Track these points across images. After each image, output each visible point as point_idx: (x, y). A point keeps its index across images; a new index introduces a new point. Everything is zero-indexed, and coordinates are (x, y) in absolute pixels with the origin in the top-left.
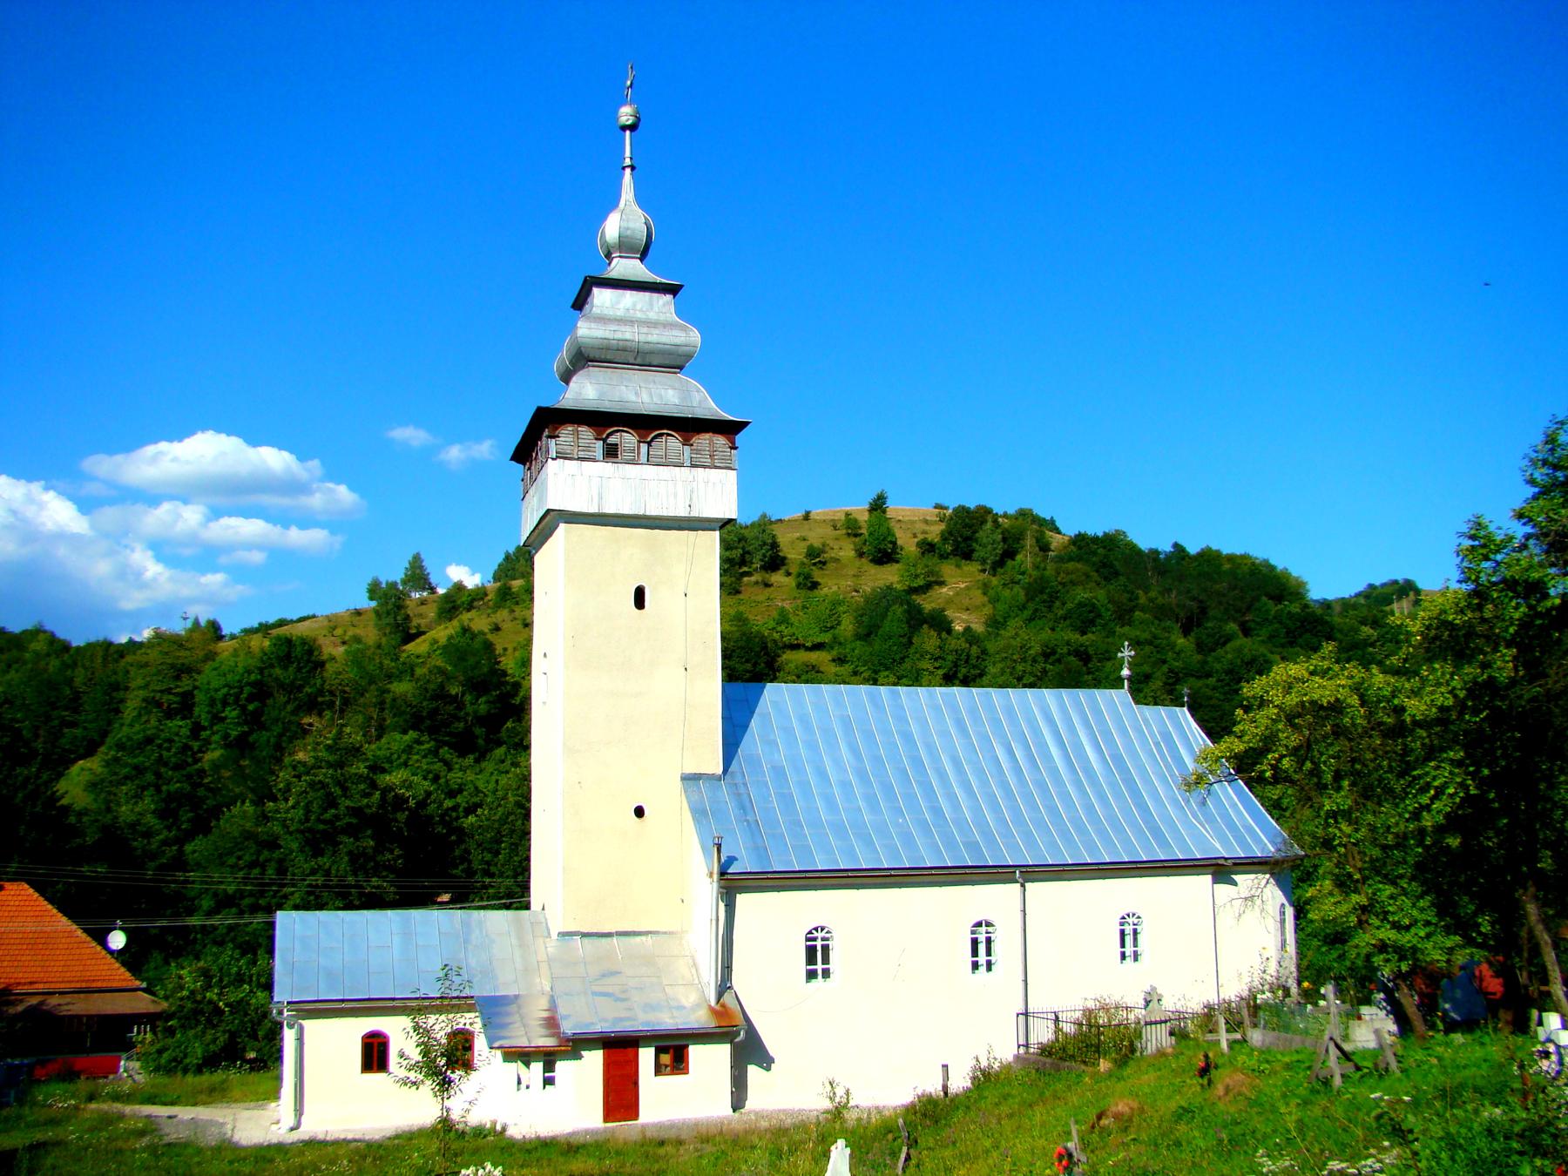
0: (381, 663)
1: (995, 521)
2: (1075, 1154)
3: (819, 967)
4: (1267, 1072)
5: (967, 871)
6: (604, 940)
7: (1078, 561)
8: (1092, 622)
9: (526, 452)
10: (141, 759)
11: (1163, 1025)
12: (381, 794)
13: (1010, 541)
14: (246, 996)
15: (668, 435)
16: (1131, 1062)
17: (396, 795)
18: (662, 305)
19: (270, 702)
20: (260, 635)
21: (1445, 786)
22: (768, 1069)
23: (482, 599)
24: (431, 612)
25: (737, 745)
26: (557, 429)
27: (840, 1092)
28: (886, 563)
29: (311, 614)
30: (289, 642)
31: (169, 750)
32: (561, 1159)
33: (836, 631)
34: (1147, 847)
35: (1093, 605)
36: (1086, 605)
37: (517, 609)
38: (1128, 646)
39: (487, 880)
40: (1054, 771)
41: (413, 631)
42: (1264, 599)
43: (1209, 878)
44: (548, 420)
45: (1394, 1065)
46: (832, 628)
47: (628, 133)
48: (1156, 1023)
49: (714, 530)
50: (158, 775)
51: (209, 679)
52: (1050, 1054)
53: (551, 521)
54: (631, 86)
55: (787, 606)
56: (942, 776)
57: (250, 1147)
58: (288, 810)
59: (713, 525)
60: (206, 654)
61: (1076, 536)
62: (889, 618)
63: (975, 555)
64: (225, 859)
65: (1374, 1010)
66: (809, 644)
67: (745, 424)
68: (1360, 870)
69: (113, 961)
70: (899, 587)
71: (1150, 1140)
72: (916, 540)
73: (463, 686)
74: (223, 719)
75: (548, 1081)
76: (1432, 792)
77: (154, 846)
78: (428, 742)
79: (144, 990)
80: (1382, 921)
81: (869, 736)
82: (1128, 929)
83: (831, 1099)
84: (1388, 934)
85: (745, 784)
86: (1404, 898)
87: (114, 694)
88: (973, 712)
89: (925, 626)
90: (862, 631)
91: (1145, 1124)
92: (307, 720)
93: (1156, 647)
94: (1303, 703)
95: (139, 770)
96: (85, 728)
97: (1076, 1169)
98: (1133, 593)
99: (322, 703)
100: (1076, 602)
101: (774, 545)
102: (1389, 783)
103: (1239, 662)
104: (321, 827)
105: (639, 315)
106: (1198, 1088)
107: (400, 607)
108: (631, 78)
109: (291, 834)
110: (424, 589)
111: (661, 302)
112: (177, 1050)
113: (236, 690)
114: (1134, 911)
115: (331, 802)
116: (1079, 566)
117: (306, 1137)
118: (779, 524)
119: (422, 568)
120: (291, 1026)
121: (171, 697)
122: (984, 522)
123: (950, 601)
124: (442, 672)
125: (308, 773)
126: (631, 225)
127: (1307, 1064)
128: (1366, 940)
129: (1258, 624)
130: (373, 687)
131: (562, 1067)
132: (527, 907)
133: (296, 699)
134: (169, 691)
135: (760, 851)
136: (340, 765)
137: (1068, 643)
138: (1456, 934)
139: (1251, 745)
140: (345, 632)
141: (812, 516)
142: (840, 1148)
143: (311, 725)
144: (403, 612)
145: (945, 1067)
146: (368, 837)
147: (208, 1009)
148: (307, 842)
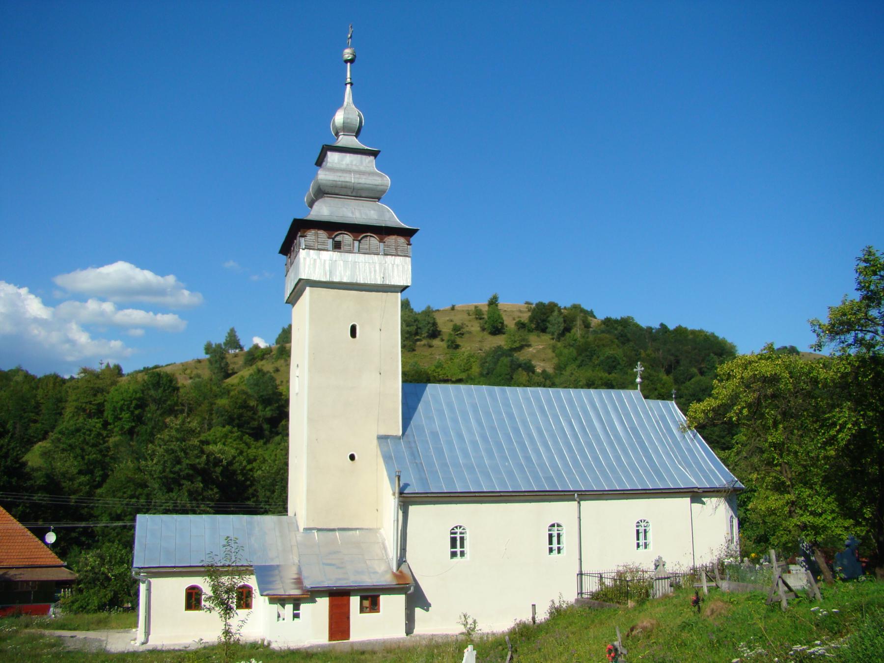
0: (211, 388)
2: (619, 649)
3: (458, 549)
5: (547, 493)
6: (331, 533)
8: (615, 367)
9: (288, 248)
10: (73, 440)
11: (666, 580)
15: (371, 236)
17: (215, 458)
18: (368, 162)
19: (147, 409)
20: (144, 373)
21: (845, 423)
22: (427, 610)
23: (269, 354)
24: (240, 361)
26: (305, 232)
27: (470, 621)
30: (159, 375)
31: (90, 435)
33: (470, 372)
34: (652, 480)
35: (615, 358)
36: (611, 358)
38: (640, 364)
39: (267, 507)
41: (230, 372)
42: (712, 355)
44: (300, 227)
45: (818, 595)
46: (467, 370)
47: (349, 64)
48: (662, 579)
49: (398, 292)
50: (83, 450)
51: (114, 396)
52: (597, 599)
53: (301, 285)
54: (351, 37)
57: (117, 653)
58: (153, 465)
61: (605, 319)
63: (548, 330)
64: (116, 493)
65: (798, 567)
66: (454, 379)
68: (790, 480)
70: (505, 347)
71: (665, 642)
73: (257, 401)
74: (120, 419)
76: (838, 427)
78: (237, 432)
79: (65, 567)
80: (804, 511)
81: (488, 414)
82: (641, 529)
83: (464, 625)
84: (807, 519)
85: (415, 442)
87: (59, 404)
88: (549, 402)
89: (520, 369)
91: (661, 633)
93: (651, 381)
94: (755, 375)
95: (72, 447)
96: (43, 424)
97: (619, 659)
98: (638, 351)
99: (177, 410)
100: (606, 356)
101: (435, 324)
102: (807, 426)
103: (698, 389)
104: (172, 476)
105: (354, 168)
106: (692, 614)
107: (223, 358)
108: (351, 32)
109: (154, 479)
110: (236, 348)
111: (367, 161)
112: (83, 601)
113: (128, 402)
114: (645, 519)
115: (179, 462)
116: (607, 336)
119: (235, 336)
120: (144, 582)
121: (91, 406)
122: (553, 311)
123: (534, 356)
124: (246, 393)
125: (165, 445)
126: (350, 116)
127: (761, 597)
129: (708, 369)
130: (206, 401)
131: (304, 607)
132: (287, 515)
133: (162, 408)
134: (90, 403)
135: (423, 481)
137: (601, 379)
138: (850, 518)
140: (192, 372)
141: (456, 307)
142: (470, 650)
144: (224, 360)
145: (534, 606)
146: (199, 481)
147: (102, 577)
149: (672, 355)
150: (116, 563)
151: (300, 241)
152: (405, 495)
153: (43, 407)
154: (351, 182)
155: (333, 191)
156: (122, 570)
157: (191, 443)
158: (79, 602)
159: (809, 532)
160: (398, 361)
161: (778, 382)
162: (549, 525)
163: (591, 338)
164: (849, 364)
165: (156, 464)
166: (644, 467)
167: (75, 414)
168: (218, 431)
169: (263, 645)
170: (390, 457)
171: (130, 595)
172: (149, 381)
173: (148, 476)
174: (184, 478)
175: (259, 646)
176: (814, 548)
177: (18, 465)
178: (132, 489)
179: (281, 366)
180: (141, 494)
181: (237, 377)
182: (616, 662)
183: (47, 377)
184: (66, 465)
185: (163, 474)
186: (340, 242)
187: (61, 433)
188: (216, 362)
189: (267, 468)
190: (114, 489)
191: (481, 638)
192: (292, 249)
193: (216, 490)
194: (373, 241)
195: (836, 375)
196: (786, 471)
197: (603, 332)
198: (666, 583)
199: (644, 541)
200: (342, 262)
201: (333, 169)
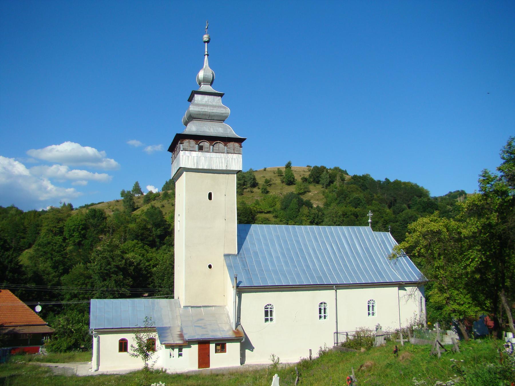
0: (125, 218)
1: (327, 171)
2: (353, 379)
3: (269, 317)
4: (416, 352)
5: (318, 286)
6: (198, 309)
7: (354, 184)
8: (359, 204)
9: (173, 148)
10: (46, 249)
11: (382, 336)
12: (125, 261)
13: (332, 178)
14: (81, 327)
15: (220, 143)
16: (371, 349)
17: (130, 261)
18: (217, 100)
19: (88, 230)
21: (475, 258)
22: (252, 351)
24: (142, 201)
25: (242, 244)
26: (183, 141)
27: (276, 358)
28: (291, 185)
30: (95, 211)
31: (55, 246)
32: (184, 381)
33: (275, 207)
34: (377, 278)
35: (359, 199)
37: (170, 200)
39: (160, 289)
40: (346, 253)
41: (136, 207)
42: (415, 197)
43: (397, 288)
44: (180, 138)
45: (458, 350)
46: (273, 206)
47: (206, 43)
48: (380, 336)
49: (235, 174)
50: (52, 254)
51: (69, 223)
52: (345, 346)
53: (181, 171)
55: (259, 199)
56: (309, 254)
57: (82, 377)
58: (95, 266)
60: (68, 215)
61: (353, 176)
63: (320, 182)
65: (451, 331)
66: (266, 211)
67: (245, 139)
68: (447, 286)
69: (37, 315)
70: (295, 193)
72: (301, 177)
74: (73, 236)
76: (470, 260)
77: (51, 278)
78: (141, 244)
80: (454, 302)
81: (285, 242)
82: (371, 305)
83: (273, 361)
84: (456, 307)
86: (461, 295)
87: (38, 228)
88: (320, 233)
89: (304, 206)
90: (283, 207)
92: (101, 236)
94: (428, 231)
97: (353, 384)
98: (372, 195)
99: (106, 231)
100: (353, 197)
101: (254, 179)
104: (106, 271)
105: (210, 103)
106: (394, 357)
107: (131, 199)
109: (95, 274)
110: (139, 193)
111: (217, 99)
112: (58, 345)
113: (78, 227)
114: (373, 299)
115: (109, 264)
116: (354, 186)
117: (101, 373)
118: (256, 172)
119: (138, 186)
121: (56, 229)
122: (323, 171)
123: (312, 197)
124: (145, 220)
125: (101, 254)
126: (207, 74)
127: (429, 349)
129: (413, 205)
131: (185, 350)
132: (173, 298)
133: (97, 229)
134: (55, 227)
135: (250, 279)
136: (112, 251)
137: (351, 211)
138: (478, 306)
139: (411, 244)
140: (113, 207)
142: (276, 377)
143: (102, 238)
144: (132, 201)
145: (310, 350)
146: (121, 275)
147: (68, 331)
148: (101, 277)
149: (392, 197)
153: (28, 229)
154: (208, 112)
156: (79, 327)
157: (116, 253)
161: (440, 234)
165: (96, 265)
168: (130, 243)
169: (163, 371)
170: (231, 267)
172: (89, 214)
173: (92, 272)
174: (113, 273)
177: (18, 267)
178: (83, 279)
180: (88, 282)
182: (351, 385)
183: (30, 212)
184: (45, 266)
185: (100, 271)
186: (203, 146)
187: (39, 245)
188: (127, 201)
189: (160, 267)
191: (282, 367)
193: (130, 280)
194: (221, 145)
195: (470, 233)
198: (382, 338)
199: (372, 311)
201: (198, 105)
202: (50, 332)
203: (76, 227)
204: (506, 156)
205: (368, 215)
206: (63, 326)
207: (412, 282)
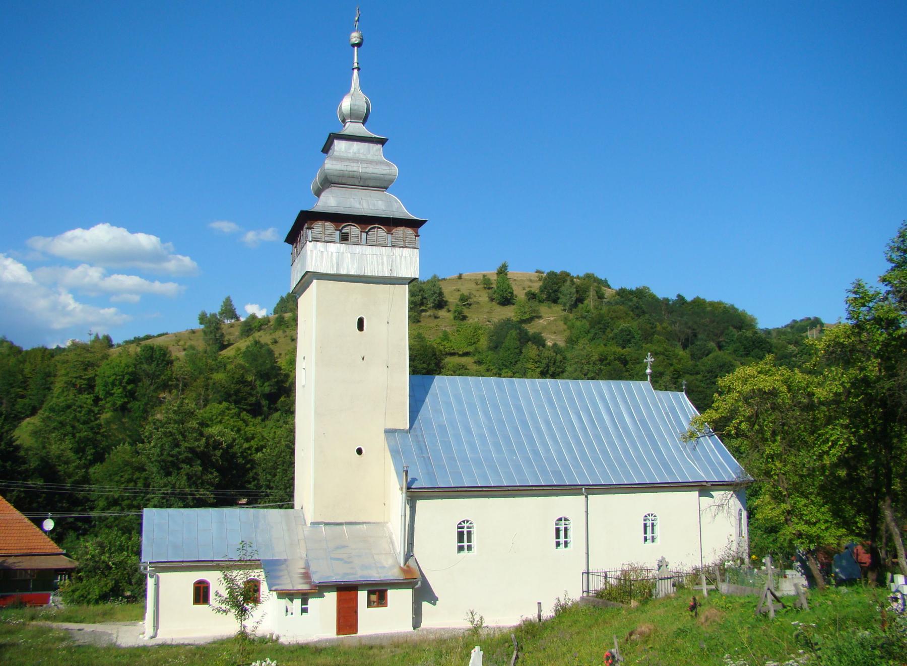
0: (206, 362)
1: (572, 281)
2: (616, 656)
3: (465, 544)
8: (629, 341)
9: (293, 237)
11: (669, 580)
12: (206, 439)
15: (378, 228)
16: (650, 602)
17: (215, 440)
18: (376, 150)
19: (140, 384)
21: (838, 440)
22: (434, 604)
24: (236, 332)
27: (477, 618)
28: (507, 305)
29: (165, 332)
31: (80, 412)
32: (311, 657)
33: (477, 345)
35: (630, 331)
37: (287, 330)
38: (650, 355)
39: (269, 491)
41: (226, 343)
42: (731, 328)
43: (697, 493)
44: (307, 218)
45: (805, 605)
46: (474, 343)
47: (356, 48)
48: (665, 579)
49: (405, 284)
50: (73, 427)
51: (105, 371)
52: (602, 597)
53: (307, 279)
55: (448, 329)
58: (151, 449)
59: (405, 281)
61: (620, 290)
62: (508, 338)
63: (560, 301)
64: (113, 477)
65: (794, 572)
66: (461, 353)
67: (425, 221)
69: (46, 537)
70: (515, 319)
72: (525, 291)
73: (255, 376)
74: (112, 394)
75: (304, 610)
76: (830, 444)
78: (234, 409)
80: (799, 520)
81: (495, 407)
82: (649, 523)
83: (471, 622)
84: (803, 528)
86: (812, 506)
87: (48, 379)
88: (558, 393)
89: (530, 343)
91: (658, 639)
92: (162, 395)
93: (667, 356)
94: (753, 390)
95: (63, 424)
96: (30, 399)
99: (171, 385)
100: (619, 329)
101: (441, 294)
104: (171, 459)
105: (362, 156)
106: (690, 618)
107: (218, 329)
108: (358, 16)
109: (152, 462)
110: (232, 318)
112: (84, 590)
113: (120, 377)
114: (652, 513)
116: (622, 307)
118: (444, 282)
119: (231, 305)
121: (82, 381)
122: (565, 281)
123: (544, 328)
124: (243, 367)
125: (162, 427)
126: (358, 103)
127: (754, 604)
128: (790, 530)
129: (727, 343)
130: (202, 376)
131: (312, 602)
133: (156, 383)
134: (80, 377)
135: (431, 475)
139: (723, 415)
141: (463, 277)
142: (476, 651)
143: (164, 398)
144: (220, 331)
145: (539, 604)
149: (690, 328)
150: (116, 551)
151: (306, 232)
152: (412, 490)
155: (340, 181)
158: (79, 591)
159: (804, 541)
160: (405, 355)
162: (556, 519)
163: (605, 310)
164: (841, 384)
165: (154, 447)
166: (652, 460)
167: (65, 390)
168: (214, 408)
169: (272, 640)
171: (130, 583)
174: (183, 462)
175: (267, 640)
176: (808, 555)
177: (12, 449)
179: (279, 337)
180: (139, 478)
181: (233, 349)
183: (34, 351)
186: (348, 233)
187: (52, 410)
188: (211, 332)
189: (268, 451)
190: (111, 472)
191: (488, 634)
192: (299, 239)
193: (215, 474)
196: (783, 482)
197: (617, 303)
198: (669, 583)
199: (651, 535)
200: (349, 255)
202: (69, 567)
203: (118, 378)
204: (896, 256)
205: (645, 360)
206: (93, 556)
207: (724, 483)
